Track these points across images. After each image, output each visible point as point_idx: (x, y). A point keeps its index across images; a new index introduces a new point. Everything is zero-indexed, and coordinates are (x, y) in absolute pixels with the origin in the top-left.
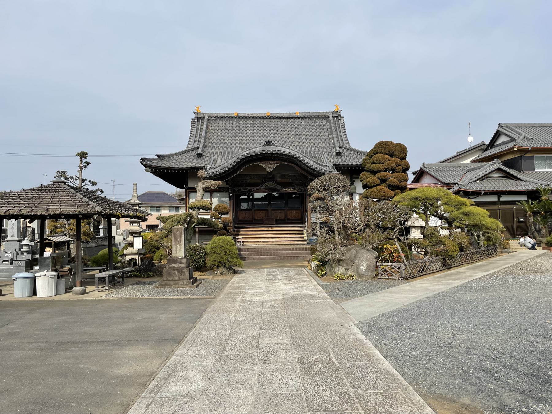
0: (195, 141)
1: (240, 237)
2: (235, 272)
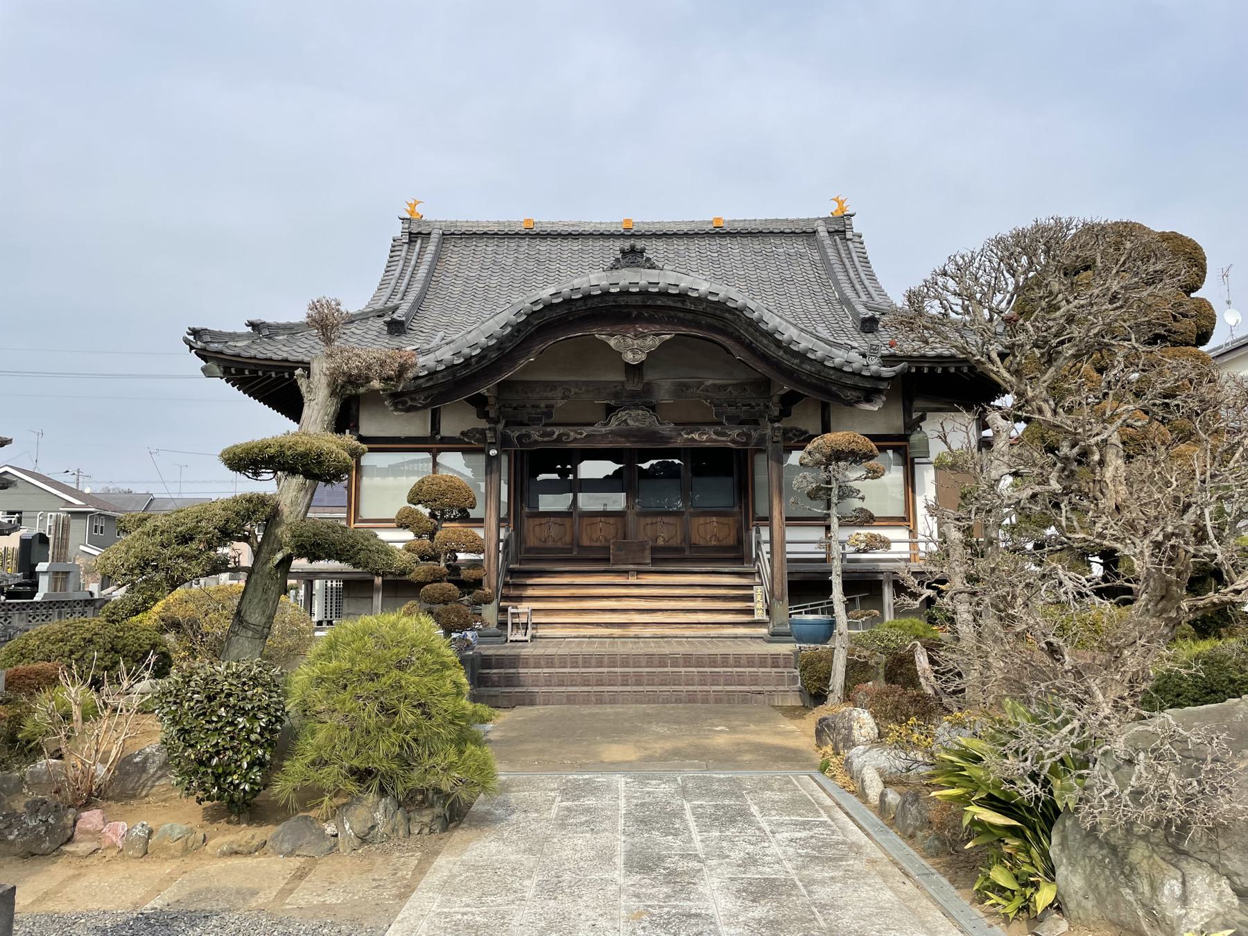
0: (394, 293)
1: (524, 607)
2: (455, 815)
